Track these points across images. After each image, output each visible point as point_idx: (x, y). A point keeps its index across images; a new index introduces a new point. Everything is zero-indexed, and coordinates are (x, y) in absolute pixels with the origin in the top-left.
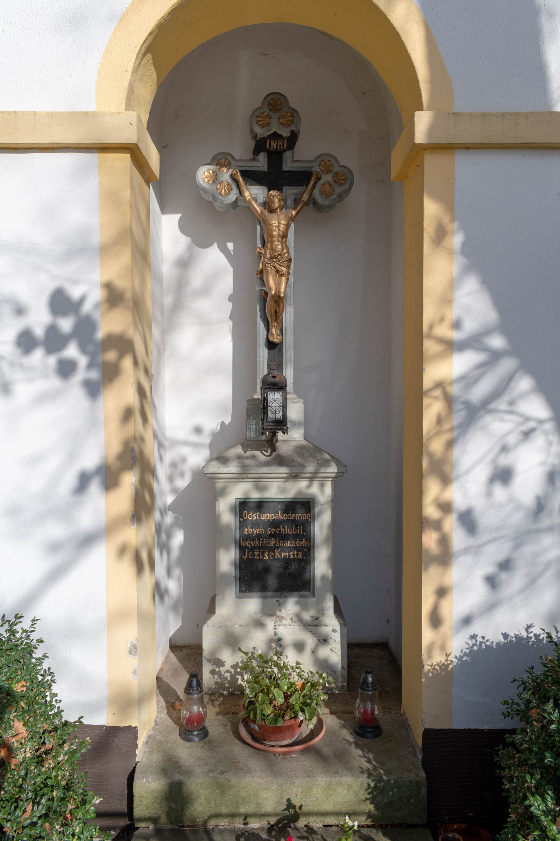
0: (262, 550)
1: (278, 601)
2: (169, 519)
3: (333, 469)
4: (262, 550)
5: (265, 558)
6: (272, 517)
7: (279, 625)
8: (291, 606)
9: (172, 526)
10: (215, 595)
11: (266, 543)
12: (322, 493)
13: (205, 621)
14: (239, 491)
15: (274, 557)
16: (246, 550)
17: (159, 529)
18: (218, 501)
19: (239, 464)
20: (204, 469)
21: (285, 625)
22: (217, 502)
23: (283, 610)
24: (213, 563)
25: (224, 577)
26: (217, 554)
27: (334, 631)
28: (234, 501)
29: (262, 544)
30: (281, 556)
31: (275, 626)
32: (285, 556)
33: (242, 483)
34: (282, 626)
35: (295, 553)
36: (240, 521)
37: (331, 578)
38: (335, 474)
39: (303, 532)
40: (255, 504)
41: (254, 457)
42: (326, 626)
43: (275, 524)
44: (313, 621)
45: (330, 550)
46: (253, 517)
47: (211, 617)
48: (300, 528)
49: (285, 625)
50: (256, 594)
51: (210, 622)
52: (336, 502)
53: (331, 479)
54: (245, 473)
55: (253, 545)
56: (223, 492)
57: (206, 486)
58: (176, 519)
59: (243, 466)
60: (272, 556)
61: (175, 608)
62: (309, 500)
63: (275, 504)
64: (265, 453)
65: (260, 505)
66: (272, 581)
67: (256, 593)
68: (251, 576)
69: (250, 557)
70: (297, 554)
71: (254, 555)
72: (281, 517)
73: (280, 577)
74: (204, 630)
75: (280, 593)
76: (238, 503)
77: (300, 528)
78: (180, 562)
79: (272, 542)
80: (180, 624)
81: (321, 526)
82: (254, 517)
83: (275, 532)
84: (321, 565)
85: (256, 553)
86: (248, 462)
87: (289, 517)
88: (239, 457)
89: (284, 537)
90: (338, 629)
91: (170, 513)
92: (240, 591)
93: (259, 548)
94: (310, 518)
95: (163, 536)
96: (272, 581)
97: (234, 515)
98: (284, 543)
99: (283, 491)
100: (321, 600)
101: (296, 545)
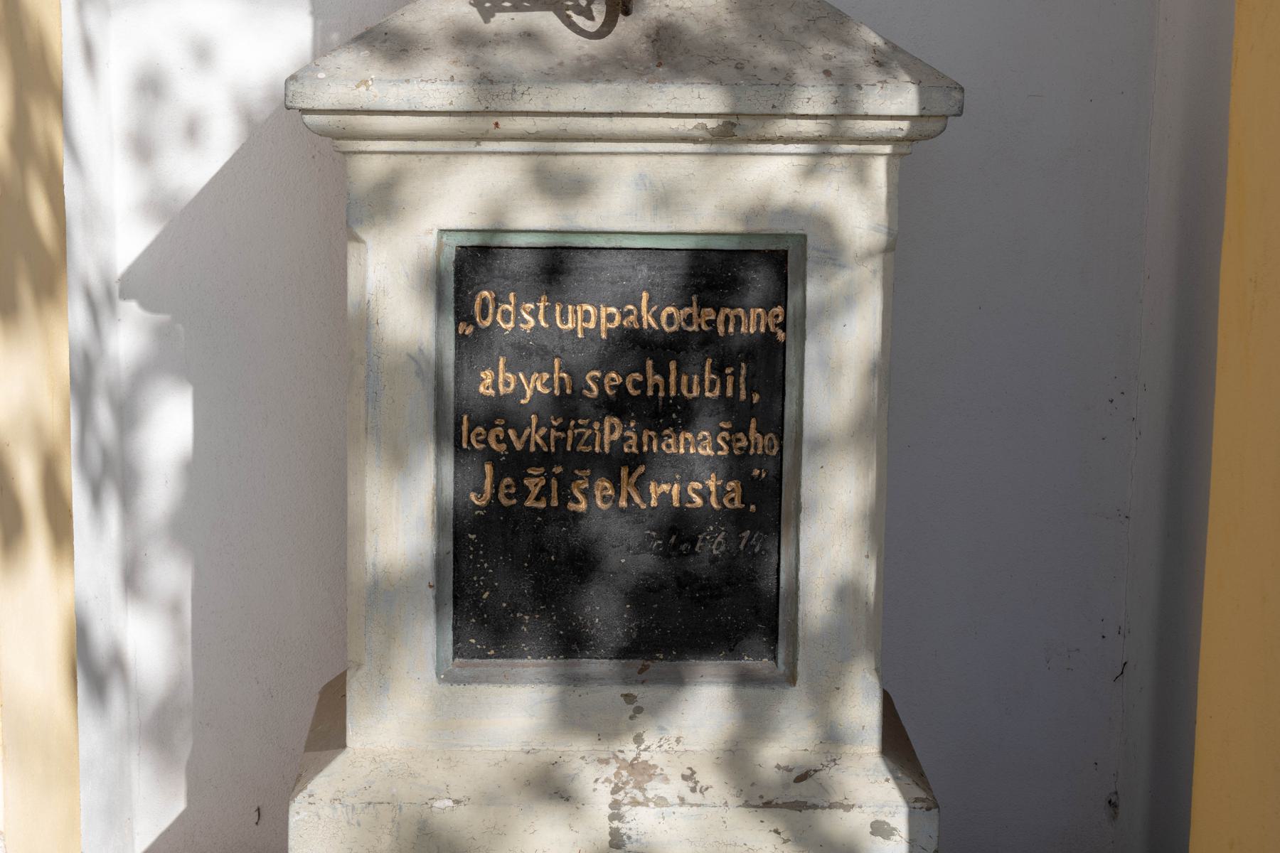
0: (558, 470)
1: (629, 698)
2: (128, 337)
3: (894, 101)
4: (558, 470)
5: (572, 506)
6: (610, 318)
7: (635, 803)
8: (704, 708)
9: (144, 374)
10: (344, 675)
11: (577, 439)
12: (856, 208)
13: (297, 781)
14: (463, 195)
15: (616, 501)
16: (488, 468)
17: (84, 379)
18: (357, 239)
19: (458, 71)
20: (293, 87)
21: (661, 802)
22: (352, 248)
23: (650, 739)
24: (337, 526)
25: (385, 594)
26: (351, 486)
27: (880, 829)
28: (431, 241)
29: (561, 442)
30: (645, 497)
31: (615, 805)
32: (665, 497)
33: (473, 162)
34: (645, 803)
35: (712, 484)
36: (460, 338)
37: (872, 599)
38: (905, 125)
39: (750, 391)
40: (529, 260)
41: (530, 37)
42: (848, 808)
43: (635, 345)
44: (785, 786)
45: (872, 475)
46: (520, 320)
47: (327, 762)
48: (736, 374)
49: (661, 802)
50: (530, 666)
51: (323, 785)
52: (900, 252)
53: (887, 149)
54: (486, 113)
55: (518, 446)
56: (384, 202)
57: (309, 170)
58: (162, 335)
59: (485, 80)
60: (605, 499)
61: (158, 730)
62: (781, 247)
63: (621, 257)
64: (579, 20)
65: (557, 266)
66: (602, 609)
67: (529, 661)
68: (512, 579)
69: (505, 502)
70: (721, 492)
71: (523, 492)
72: (648, 320)
73: (642, 596)
74: (293, 820)
75: (639, 663)
76: (450, 254)
77: (736, 374)
78: (182, 529)
79: (610, 432)
80: (180, 806)
81: (842, 352)
82: (522, 317)
83: (621, 389)
84: (832, 543)
85: (534, 484)
86: (506, 58)
87: (689, 320)
88: (464, 39)
89: (672, 414)
90: (899, 820)
91: (131, 310)
92: (457, 653)
93: (544, 459)
94: (783, 326)
95: (103, 415)
96: (602, 609)
97: (431, 307)
98: (661, 438)
99: (663, 199)
100: (826, 694)
101: (717, 448)
